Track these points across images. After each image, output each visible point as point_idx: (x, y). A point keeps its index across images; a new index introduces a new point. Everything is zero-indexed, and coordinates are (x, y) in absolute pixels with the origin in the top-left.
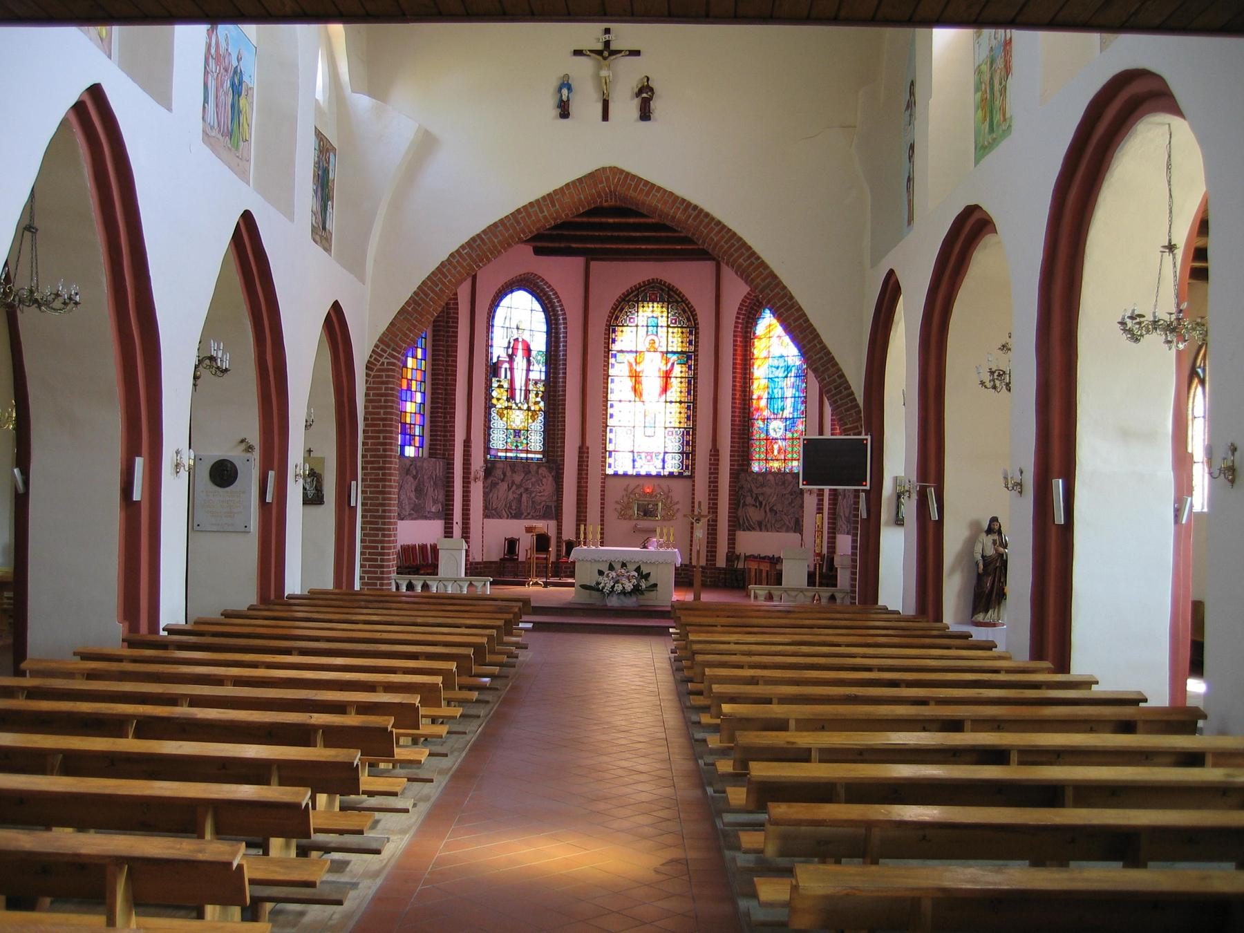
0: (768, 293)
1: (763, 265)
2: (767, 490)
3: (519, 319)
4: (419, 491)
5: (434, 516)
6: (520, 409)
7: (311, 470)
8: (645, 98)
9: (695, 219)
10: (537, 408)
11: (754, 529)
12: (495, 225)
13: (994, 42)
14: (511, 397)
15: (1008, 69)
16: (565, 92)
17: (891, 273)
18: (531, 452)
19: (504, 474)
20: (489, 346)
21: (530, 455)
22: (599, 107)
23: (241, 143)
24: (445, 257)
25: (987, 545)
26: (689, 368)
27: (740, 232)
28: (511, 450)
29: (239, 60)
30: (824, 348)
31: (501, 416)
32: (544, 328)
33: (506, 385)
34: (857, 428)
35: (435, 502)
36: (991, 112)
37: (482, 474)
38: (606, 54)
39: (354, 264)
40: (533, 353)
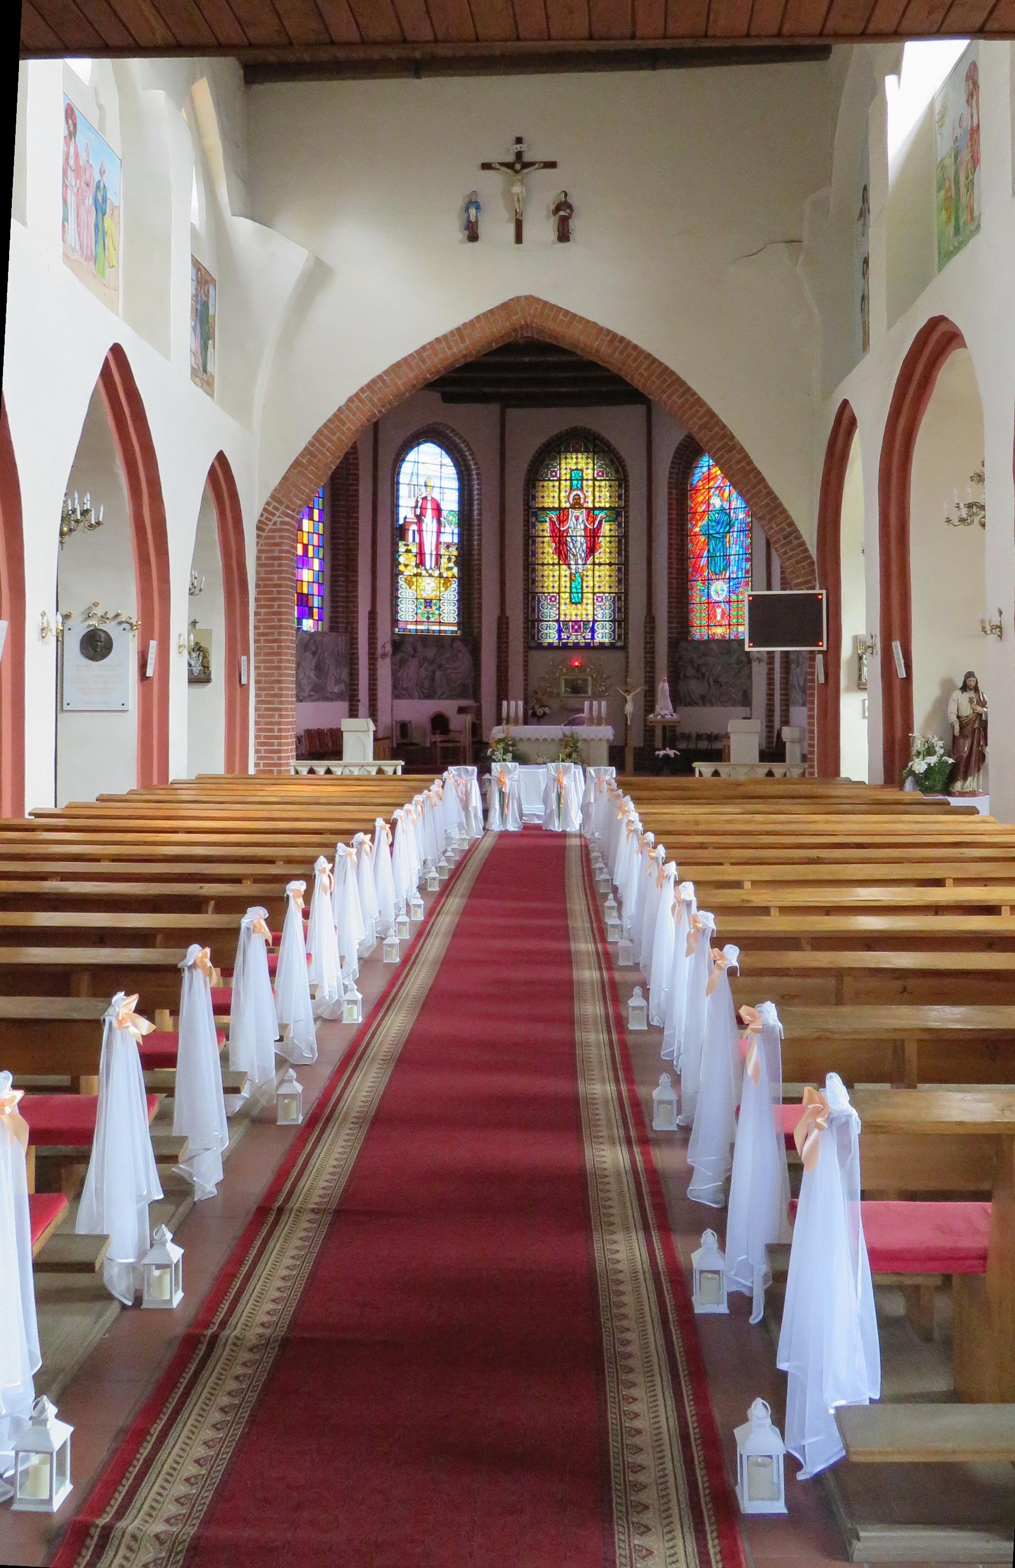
0: (702, 438)
1: (699, 402)
2: (711, 660)
3: (428, 474)
4: (319, 669)
5: (338, 697)
6: (430, 575)
7: (197, 644)
8: (563, 216)
9: (621, 353)
10: (450, 574)
11: (696, 704)
12: (398, 365)
13: (958, 132)
14: (421, 563)
15: (975, 160)
16: (473, 211)
17: (845, 403)
18: (445, 624)
19: (415, 650)
20: (395, 506)
21: (443, 628)
22: (512, 228)
23: (108, 270)
24: (342, 401)
25: (962, 704)
26: (619, 525)
27: (672, 367)
28: (422, 623)
29: (102, 173)
30: (770, 492)
31: (410, 584)
32: (455, 484)
33: (414, 549)
34: (809, 581)
35: (338, 682)
36: (957, 212)
37: (389, 648)
38: (518, 166)
39: (239, 408)
40: (444, 513)
